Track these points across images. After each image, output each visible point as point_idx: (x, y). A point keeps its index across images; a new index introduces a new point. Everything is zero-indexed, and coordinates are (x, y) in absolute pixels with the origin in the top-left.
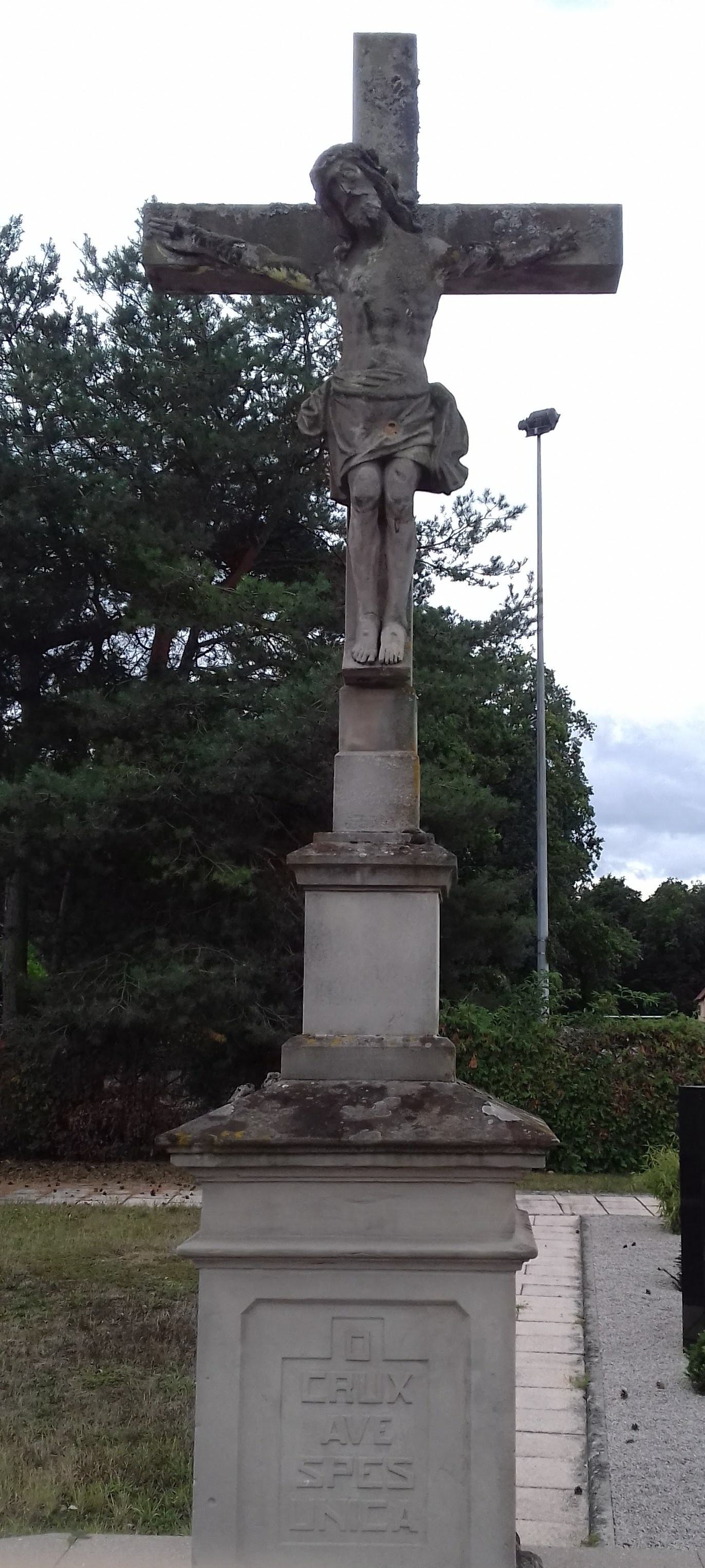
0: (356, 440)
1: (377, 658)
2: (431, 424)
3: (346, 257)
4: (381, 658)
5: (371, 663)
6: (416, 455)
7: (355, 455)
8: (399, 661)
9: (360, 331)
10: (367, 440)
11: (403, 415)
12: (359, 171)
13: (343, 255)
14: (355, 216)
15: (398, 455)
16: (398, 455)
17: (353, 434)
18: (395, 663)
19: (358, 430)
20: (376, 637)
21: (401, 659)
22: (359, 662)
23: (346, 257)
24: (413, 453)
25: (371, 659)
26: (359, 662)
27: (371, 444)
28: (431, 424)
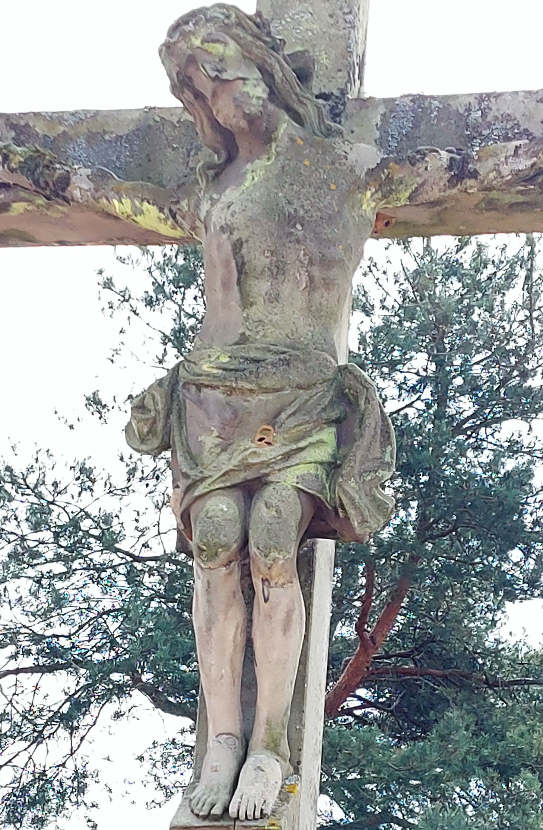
0: (206, 457)
1: (226, 810)
2: (333, 430)
3: (217, 175)
4: (232, 810)
5: (217, 818)
6: (302, 478)
7: (203, 479)
8: (263, 815)
9: (226, 286)
10: (224, 457)
11: (283, 416)
12: (232, 44)
13: (211, 172)
14: (226, 112)
15: (271, 478)
16: (271, 478)
17: (201, 444)
18: (255, 819)
19: (210, 441)
20: (233, 773)
21: (267, 811)
22: (197, 815)
23: (217, 175)
24: (290, 479)
25: (217, 810)
26: (197, 815)
27: (228, 462)
28: (333, 430)
